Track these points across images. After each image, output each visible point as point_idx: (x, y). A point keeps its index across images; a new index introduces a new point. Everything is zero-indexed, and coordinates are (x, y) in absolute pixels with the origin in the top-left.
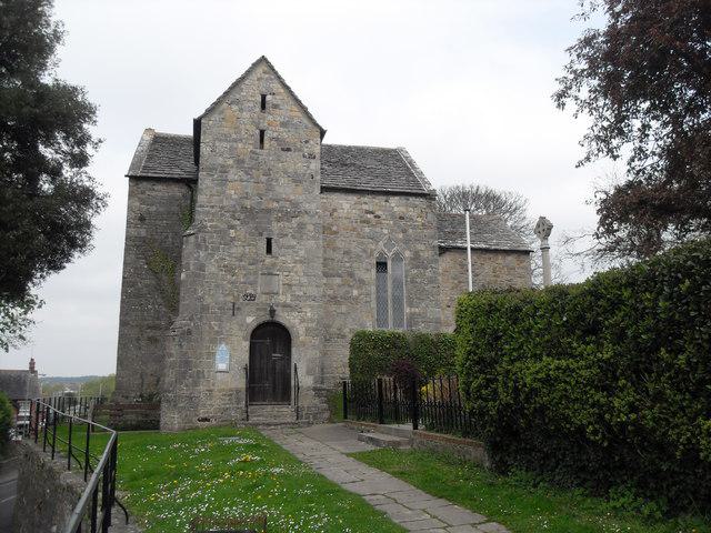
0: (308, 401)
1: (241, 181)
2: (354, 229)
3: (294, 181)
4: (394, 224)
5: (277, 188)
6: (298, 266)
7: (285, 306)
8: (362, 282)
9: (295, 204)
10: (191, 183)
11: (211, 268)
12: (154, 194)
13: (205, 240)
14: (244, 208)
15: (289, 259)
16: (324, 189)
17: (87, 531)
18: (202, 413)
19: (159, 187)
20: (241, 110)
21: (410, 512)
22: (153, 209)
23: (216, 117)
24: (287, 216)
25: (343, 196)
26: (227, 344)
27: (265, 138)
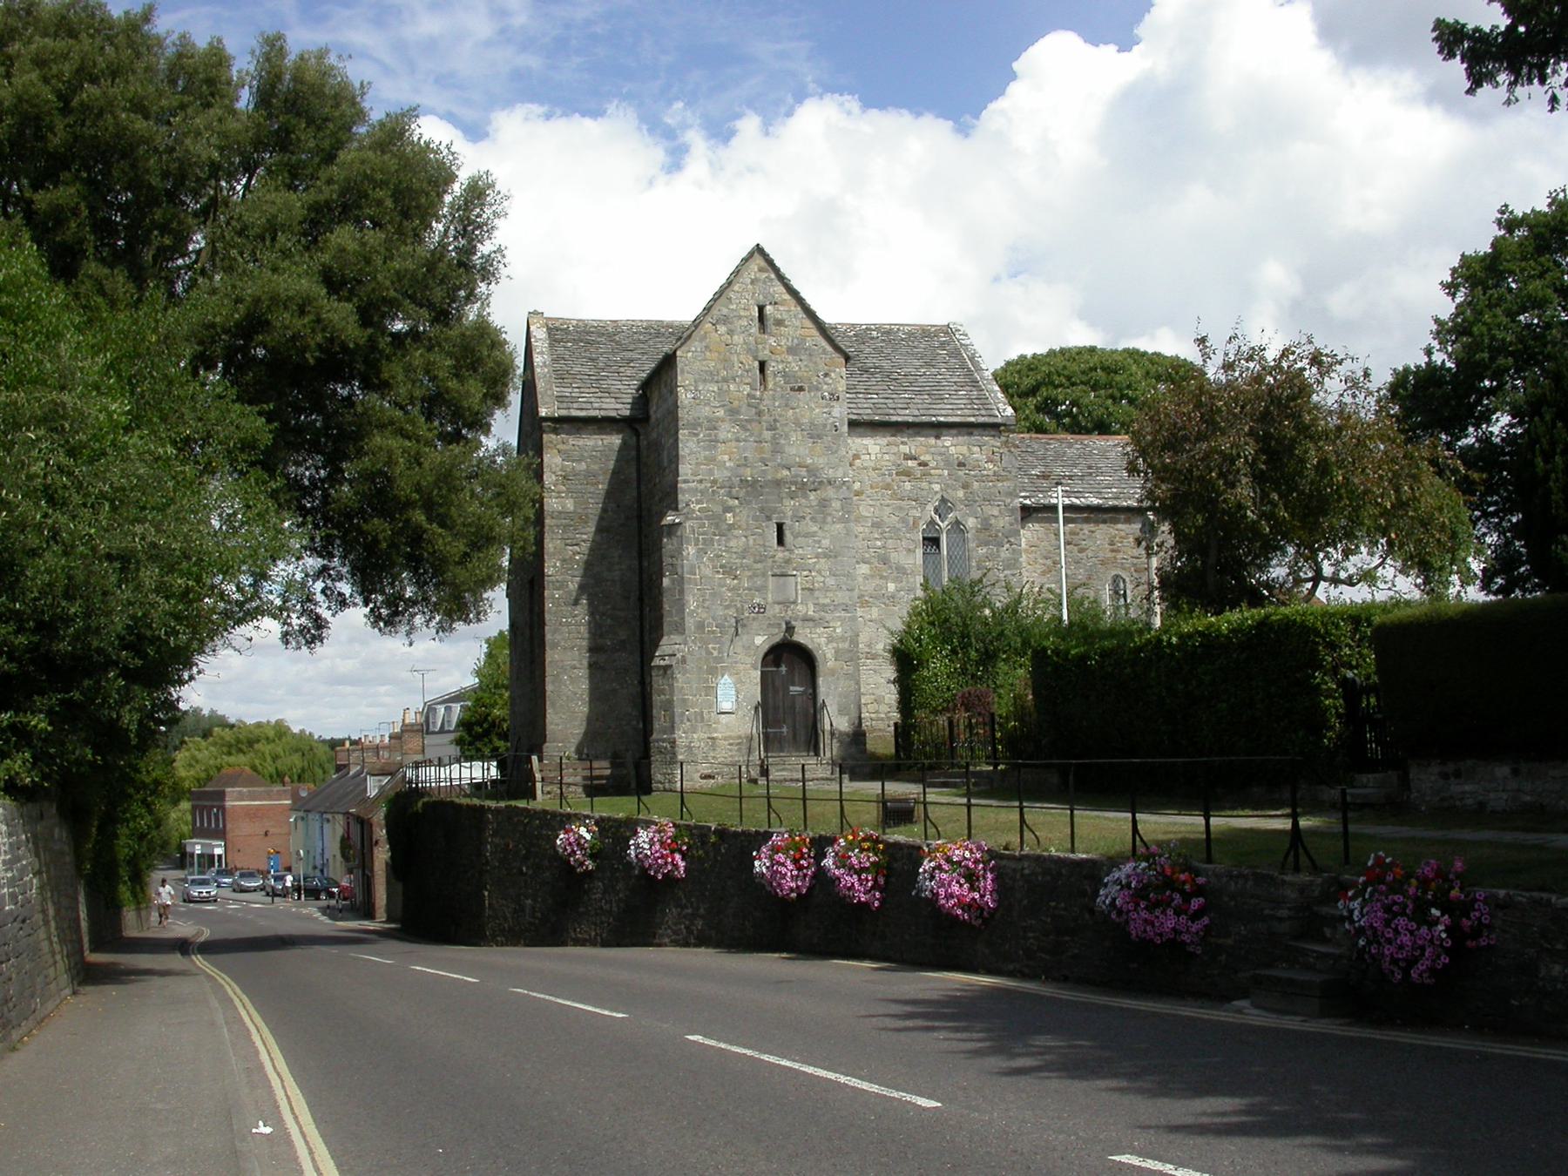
1: (738, 440)
2: (888, 487)
5: (787, 449)
6: (822, 561)
7: (806, 619)
8: (901, 570)
9: (812, 471)
17: (1539, 816)
18: (705, 768)
20: (731, 332)
22: (583, 466)
26: (730, 675)
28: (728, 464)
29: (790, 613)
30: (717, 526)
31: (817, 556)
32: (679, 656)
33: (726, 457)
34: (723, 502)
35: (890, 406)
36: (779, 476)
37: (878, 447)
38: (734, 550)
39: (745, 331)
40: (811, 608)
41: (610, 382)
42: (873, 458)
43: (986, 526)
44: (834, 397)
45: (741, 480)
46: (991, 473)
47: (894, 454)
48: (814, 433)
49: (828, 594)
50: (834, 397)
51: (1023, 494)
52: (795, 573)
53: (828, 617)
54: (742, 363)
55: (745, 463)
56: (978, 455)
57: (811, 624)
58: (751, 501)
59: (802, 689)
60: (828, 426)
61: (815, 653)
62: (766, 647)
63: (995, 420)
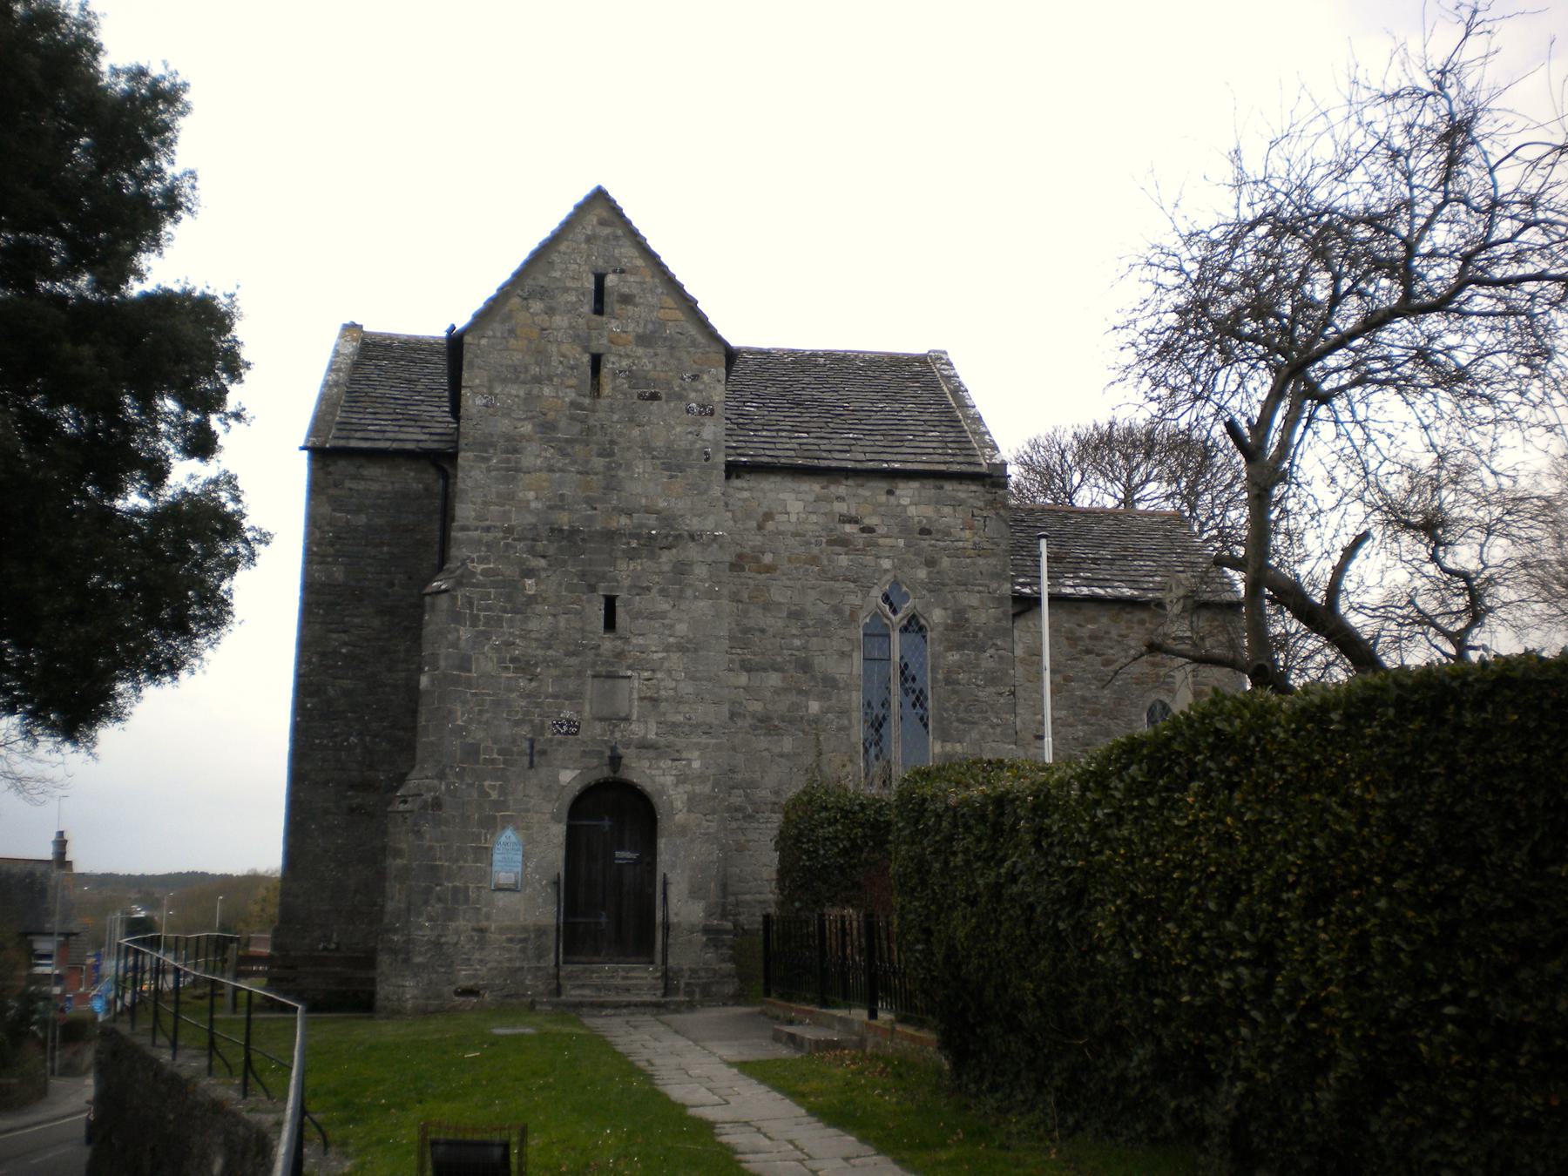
0: (688, 955)
1: (551, 470)
2: (814, 560)
3: (667, 467)
4: (908, 546)
6: (675, 656)
7: (644, 746)
8: (830, 682)
9: (667, 519)
10: (442, 461)
11: (485, 664)
12: (361, 486)
13: (471, 604)
14: (556, 532)
15: (652, 641)
16: (733, 470)
18: (464, 976)
19: (373, 471)
20: (550, 311)
21: (767, 1142)
22: (362, 519)
23: (496, 329)
24: (650, 545)
25: (789, 483)
26: (517, 829)
27: (604, 371)
28: (533, 505)
29: (618, 735)
30: (509, 598)
31: (667, 649)
32: (429, 796)
33: (531, 495)
34: (521, 562)
35: (823, 447)
36: (614, 525)
37: (801, 504)
38: (533, 635)
39: (572, 309)
40: (653, 727)
41: (423, 408)
42: (793, 518)
43: (959, 620)
44: (707, 411)
45: (552, 530)
46: (969, 545)
47: (825, 514)
48: (673, 463)
49: (682, 708)
50: (707, 411)
51: (1021, 580)
52: (629, 673)
53: (680, 742)
54: (564, 356)
55: (559, 504)
56: (949, 518)
57: (652, 753)
58: (565, 562)
59: (634, 856)
60: (695, 454)
61: (655, 800)
62: (577, 788)
63: (977, 469)
